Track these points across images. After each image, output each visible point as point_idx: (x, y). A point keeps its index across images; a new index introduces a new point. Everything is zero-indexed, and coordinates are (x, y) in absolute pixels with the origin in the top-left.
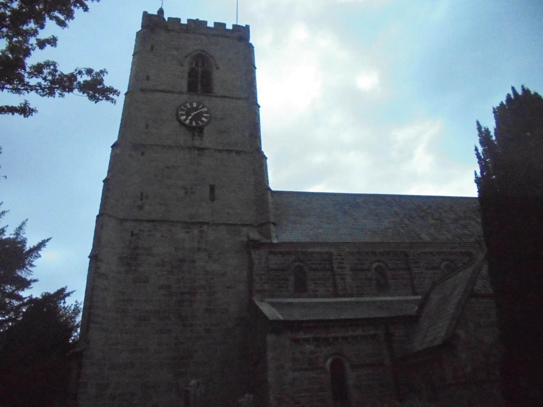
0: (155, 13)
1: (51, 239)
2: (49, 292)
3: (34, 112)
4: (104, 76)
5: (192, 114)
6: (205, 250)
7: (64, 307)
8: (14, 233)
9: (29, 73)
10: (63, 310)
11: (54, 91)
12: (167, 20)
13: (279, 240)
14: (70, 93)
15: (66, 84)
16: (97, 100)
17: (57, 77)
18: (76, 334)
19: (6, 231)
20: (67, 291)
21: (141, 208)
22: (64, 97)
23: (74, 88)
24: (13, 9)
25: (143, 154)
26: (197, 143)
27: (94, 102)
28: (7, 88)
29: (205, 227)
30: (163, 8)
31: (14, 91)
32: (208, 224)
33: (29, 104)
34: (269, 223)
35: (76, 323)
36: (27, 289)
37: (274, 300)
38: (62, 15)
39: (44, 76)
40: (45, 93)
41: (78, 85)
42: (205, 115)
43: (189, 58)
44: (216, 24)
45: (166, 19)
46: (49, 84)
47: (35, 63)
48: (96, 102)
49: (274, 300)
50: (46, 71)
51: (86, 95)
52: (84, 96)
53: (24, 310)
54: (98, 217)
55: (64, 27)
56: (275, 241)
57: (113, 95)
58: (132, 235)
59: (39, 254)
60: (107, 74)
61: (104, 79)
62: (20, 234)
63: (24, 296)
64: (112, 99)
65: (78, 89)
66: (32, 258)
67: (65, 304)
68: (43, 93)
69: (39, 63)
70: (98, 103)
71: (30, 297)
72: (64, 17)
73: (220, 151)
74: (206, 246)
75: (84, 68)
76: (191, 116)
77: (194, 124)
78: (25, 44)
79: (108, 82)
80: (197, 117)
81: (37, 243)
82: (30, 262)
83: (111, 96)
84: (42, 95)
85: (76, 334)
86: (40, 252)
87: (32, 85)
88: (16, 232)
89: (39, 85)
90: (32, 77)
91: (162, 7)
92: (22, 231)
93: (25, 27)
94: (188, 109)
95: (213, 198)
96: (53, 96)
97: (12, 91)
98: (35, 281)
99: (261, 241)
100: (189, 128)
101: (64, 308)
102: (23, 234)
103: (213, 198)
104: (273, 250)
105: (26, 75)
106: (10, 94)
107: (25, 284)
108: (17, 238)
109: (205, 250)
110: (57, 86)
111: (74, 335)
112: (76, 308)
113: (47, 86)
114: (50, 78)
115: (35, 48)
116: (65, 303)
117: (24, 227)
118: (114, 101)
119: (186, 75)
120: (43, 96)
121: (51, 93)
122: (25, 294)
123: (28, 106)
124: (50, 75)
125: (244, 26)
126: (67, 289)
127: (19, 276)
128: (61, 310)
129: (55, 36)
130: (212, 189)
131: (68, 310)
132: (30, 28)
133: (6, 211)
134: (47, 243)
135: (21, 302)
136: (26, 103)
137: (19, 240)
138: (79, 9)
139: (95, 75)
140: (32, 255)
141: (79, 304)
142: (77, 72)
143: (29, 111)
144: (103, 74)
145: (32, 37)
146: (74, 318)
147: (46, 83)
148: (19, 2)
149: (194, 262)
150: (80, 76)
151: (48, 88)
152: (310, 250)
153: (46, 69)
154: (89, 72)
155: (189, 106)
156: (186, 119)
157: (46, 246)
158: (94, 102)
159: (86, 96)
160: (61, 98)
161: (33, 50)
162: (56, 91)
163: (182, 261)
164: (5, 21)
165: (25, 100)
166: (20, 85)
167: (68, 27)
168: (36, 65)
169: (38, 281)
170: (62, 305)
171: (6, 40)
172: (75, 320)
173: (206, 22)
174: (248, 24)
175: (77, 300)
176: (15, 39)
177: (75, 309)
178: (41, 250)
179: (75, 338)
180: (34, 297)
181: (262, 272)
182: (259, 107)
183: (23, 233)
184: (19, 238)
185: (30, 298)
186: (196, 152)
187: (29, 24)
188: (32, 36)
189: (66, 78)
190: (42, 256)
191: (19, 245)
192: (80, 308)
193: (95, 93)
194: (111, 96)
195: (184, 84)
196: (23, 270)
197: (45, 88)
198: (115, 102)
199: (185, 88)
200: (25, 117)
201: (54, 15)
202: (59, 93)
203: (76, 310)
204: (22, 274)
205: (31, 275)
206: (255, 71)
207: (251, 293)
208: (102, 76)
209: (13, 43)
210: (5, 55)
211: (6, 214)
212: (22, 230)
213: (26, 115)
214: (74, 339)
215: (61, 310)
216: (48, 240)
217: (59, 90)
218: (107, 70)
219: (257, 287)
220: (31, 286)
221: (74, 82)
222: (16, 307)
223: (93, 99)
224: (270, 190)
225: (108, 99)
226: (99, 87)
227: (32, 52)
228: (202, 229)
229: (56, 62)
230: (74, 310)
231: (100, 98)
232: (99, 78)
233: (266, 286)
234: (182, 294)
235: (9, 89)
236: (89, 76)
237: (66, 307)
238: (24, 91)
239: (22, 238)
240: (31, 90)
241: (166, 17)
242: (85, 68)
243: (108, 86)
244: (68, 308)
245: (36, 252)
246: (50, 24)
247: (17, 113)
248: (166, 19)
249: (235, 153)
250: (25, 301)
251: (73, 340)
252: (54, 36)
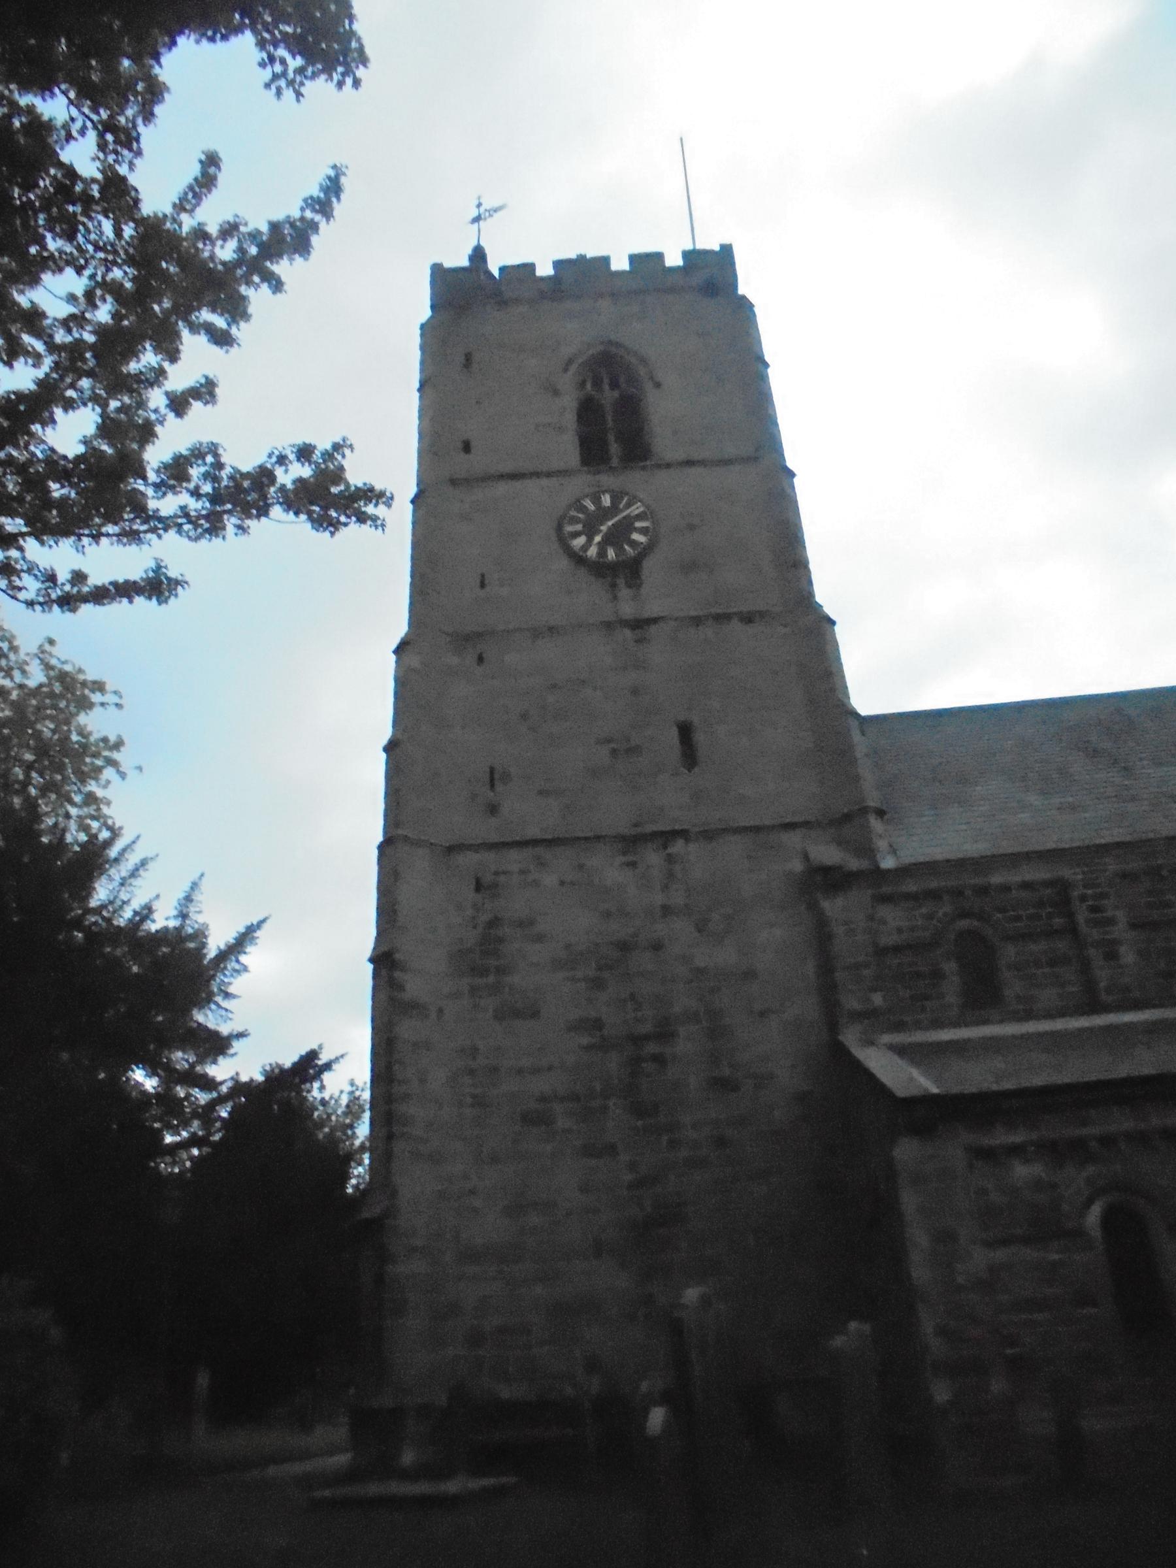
1: (268, 921)
2: (280, 1062)
3: (179, 588)
4: (344, 456)
5: (604, 528)
7: (323, 1099)
8: (175, 913)
9: (157, 486)
10: (321, 1108)
11: (222, 521)
12: (496, 273)
14: (263, 519)
15: (249, 498)
16: (334, 526)
17: (225, 483)
18: (360, 1169)
19: (156, 910)
20: (323, 1058)
21: (493, 809)
22: (249, 533)
23: (273, 504)
24: (100, 324)
25: (481, 659)
26: (627, 609)
27: (327, 534)
28: (108, 535)
29: (678, 847)
30: (482, 243)
31: (125, 540)
32: (683, 834)
33: (166, 567)
34: (864, 811)
35: (357, 1143)
36: (224, 1057)
37: (919, 1037)
38: (222, 315)
39: (192, 486)
40: (200, 530)
41: (280, 495)
42: (638, 524)
43: (573, 368)
45: (496, 273)
46: (208, 505)
47: (167, 457)
48: (332, 534)
49: (919, 1037)
50: (195, 472)
51: (303, 517)
52: (300, 522)
53: (224, 1114)
54: (381, 847)
55: (228, 348)
56: (888, 863)
57: (376, 505)
58: (479, 887)
59: (243, 964)
60: (352, 451)
61: (346, 467)
62: (190, 915)
63: (219, 1079)
64: (374, 519)
65: (281, 504)
66: (225, 975)
67: (323, 1091)
68: (196, 530)
69: (177, 453)
70: (337, 535)
71: (235, 1079)
72: (226, 320)
73: (697, 621)
75: (291, 446)
76: (601, 535)
77: (611, 554)
78: (140, 412)
79: (356, 475)
80: (617, 536)
81: (235, 935)
82: (223, 988)
83: (370, 509)
84: (193, 537)
85: (360, 1172)
86: (243, 959)
87: (167, 515)
88: (181, 912)
89: (184, 511)
90: (165, 494)
92: (192, 907)
93: (133, 367)
95: (689, 755)
96: (221, 536)
97: (119, 541)
98: (241, 1035)
100: (599, 569)
101: (324, 1102)
102: (197, 915)
103: (689, 755)
104: (886, 889)
105: (150, 492)
106: (119, 550)
107: (217, 1045)
108: (182, 926)
110: (229, 506)
111: (356, 1172)
112: (354, 1100)
113: (204, 512)
114: (207, 488)
115: (166, 418)
116: (322, 1088)
117: (197, 897)
118: (379, 522)
119: (570, 419)
120: (197, 539)
121: (212, 525)
122: (221, 1070)
123: (165, 574)
124: (208, 482)
125: (717, 248)
126: (323, 1050)
127: (199, 1024)
128: (317, 1109)
129: (211, 376)
130: (685, 731)
131: (334, 1107)
132: (145, 367)
133: (152, 858)
134: (258, 934)
135: (215, 1095)
136: (158, 569)
137: (190, 931)
138: (259, 289)
139: (321, 461)
140: (225, 968)
141: (360, 1089)
142: (274, 459)
143: (169, 584)
144: (341, 452)
145: (153, 389)
146: (351, 1126)
147: (199, 505)
148: (113, 305)
150: (283, 468)
151: (207, 517)
152: (996, 879)
153: (195, 466)
154: (305, 453)
155: (592, 507)
157: (257, 941)
158: (327, 534)
159: (304, 522)
160: (243, 538)
161: (161, 423)
162: (226, 522)
163: (624, 947)
164: (85, 360)
165: (155, 558)
166: (138, 521)
167: (239, 345)
168: (171, 461)
169: (249, 1034)
170: (315, 1093)
171: (93, 410)
172: (354, 1133)
174: (726, 241)
175: (352, 1080)
176: (114, 404)
177: (351, 1104)
178: (245, 953)
179: (361, 1181)
180: (244, 1078)
181: (861, 959)
182: (792, 474)
183: (196, 912)
184: (189, 925)
185: (233, 1082)
187: (141, 356)
188: (152, 385)
189: (249, 482)
190: (250, 968)
191: (192, 945)
192: (365, 1100)
193: (325, 508)
194: (370, 509)
195: (567, 449)
196: (210, 1009)
197: (199, 517)
198: (383, 526)
199: (572, 456)
200: (160, 603)
201: (201, 321)
202: (235, 526)
203: (355, 1104)
204: (206, 1018)
205: (229, 1021)
207: (833, 1027)
208: (339, 457)
209: (112, 416)
210: (94, 449)
211: (151, 866)
212: (193, 904)
213: (163, 598)
214: (358, 1184)
215: (317, 1109)
216: (261, 923)
217: (234, 516)
218: (352, 440)
219: (852, 1003)
220: (232, 1051)
221: (269, 486)
222: (203, 1107)
223: (325, 526)
224: (855, 715)
225: (362, 518)
226: (335, 490)
227: (158, 429)
228: (669, 850)
229: (218, 444)
230: (348, 1106)
231: (343, 519)
232: (332, 467)
233: (877, 999)
235: (114, 535)
236: (307, 464)
237: (327, 1098)
238: (149, 536)
239: (196, 926)
240: (166, 530)
242: (293, 446)
243: (360, 485)
244: (333, 1102)
245: (233, 958)
246: (192, 344)
247: (138, 595)
248: (496, 273)
250: (224, 1089)
251: (356, 1187)
252: (207, 378)
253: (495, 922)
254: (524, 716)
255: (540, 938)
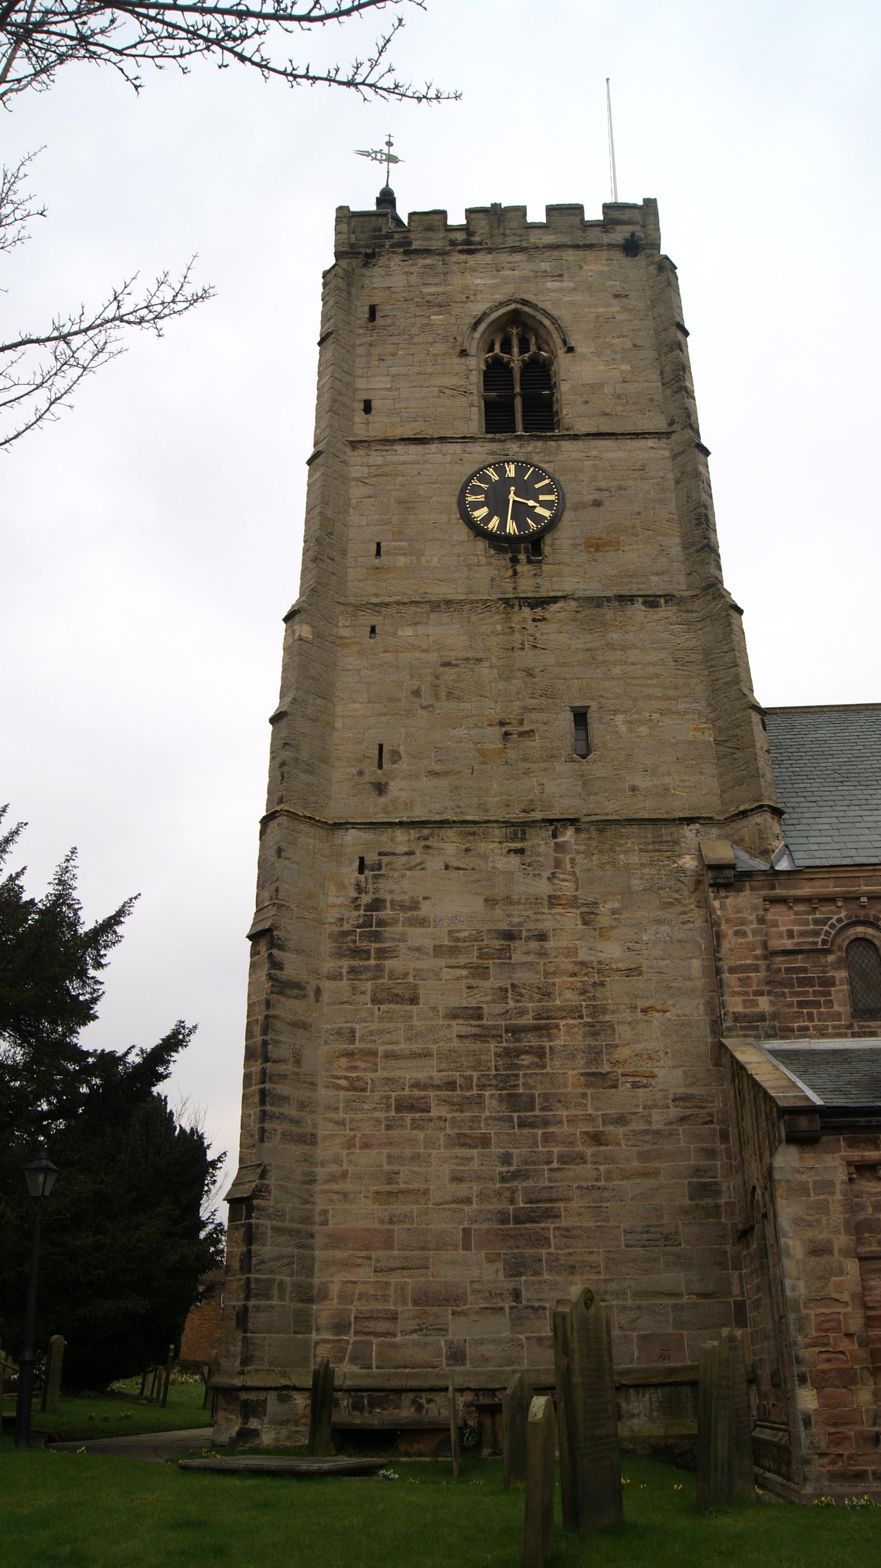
0: (371, 206)
6: (574, 902)
12: (405, 220)
13: (796, 861)
21: (380, 788)
26: (527, 586)
29: (568, 835)
44: (551, 210)
56: (783, 865)
58: (362, 868)
74: (577, 890)
86: (119, 929)
91: (387, 185)
94: (493, 485)
99: (742, 867)
109: (574, 902)
119: (476, 379)
130: (581, 717)
149: (542, 937)
155: (495, 478)
156: (503, 525)
163: (509, 936)
169: (97, 1017)
173: (521, 211)
186: (526, 611)
206: (686, 343)
228: (560, 840)
233: (764, 1004)
234: (515, 1031)
241: (403, 212)
249: (644, 603)
253: (377, 904)
254: (417, 693)
255: (422, 922)
